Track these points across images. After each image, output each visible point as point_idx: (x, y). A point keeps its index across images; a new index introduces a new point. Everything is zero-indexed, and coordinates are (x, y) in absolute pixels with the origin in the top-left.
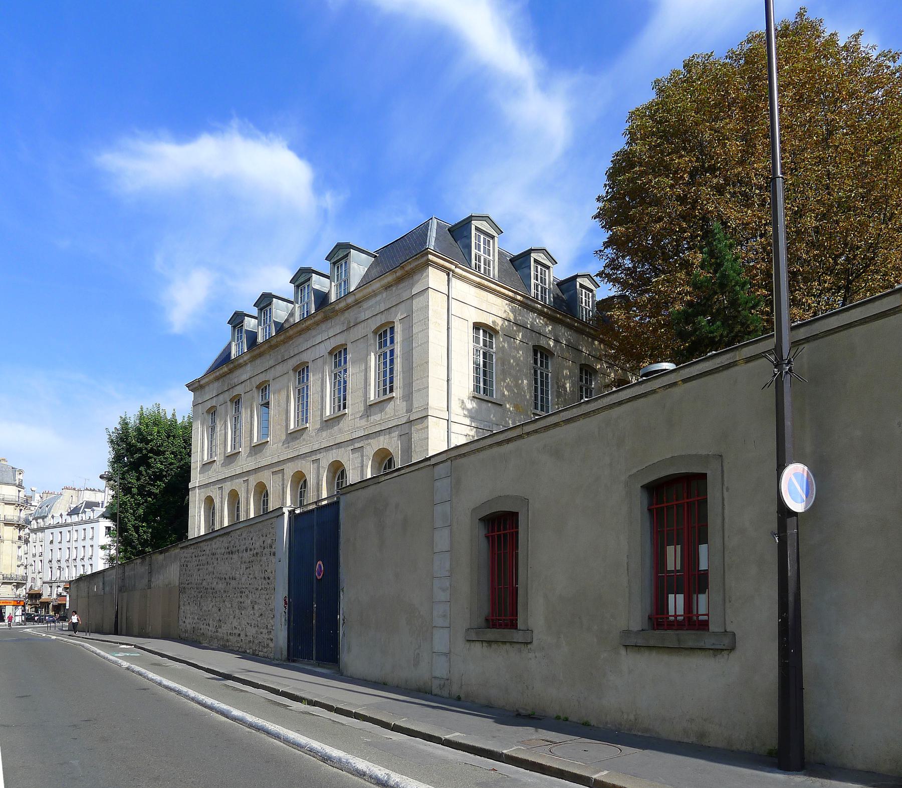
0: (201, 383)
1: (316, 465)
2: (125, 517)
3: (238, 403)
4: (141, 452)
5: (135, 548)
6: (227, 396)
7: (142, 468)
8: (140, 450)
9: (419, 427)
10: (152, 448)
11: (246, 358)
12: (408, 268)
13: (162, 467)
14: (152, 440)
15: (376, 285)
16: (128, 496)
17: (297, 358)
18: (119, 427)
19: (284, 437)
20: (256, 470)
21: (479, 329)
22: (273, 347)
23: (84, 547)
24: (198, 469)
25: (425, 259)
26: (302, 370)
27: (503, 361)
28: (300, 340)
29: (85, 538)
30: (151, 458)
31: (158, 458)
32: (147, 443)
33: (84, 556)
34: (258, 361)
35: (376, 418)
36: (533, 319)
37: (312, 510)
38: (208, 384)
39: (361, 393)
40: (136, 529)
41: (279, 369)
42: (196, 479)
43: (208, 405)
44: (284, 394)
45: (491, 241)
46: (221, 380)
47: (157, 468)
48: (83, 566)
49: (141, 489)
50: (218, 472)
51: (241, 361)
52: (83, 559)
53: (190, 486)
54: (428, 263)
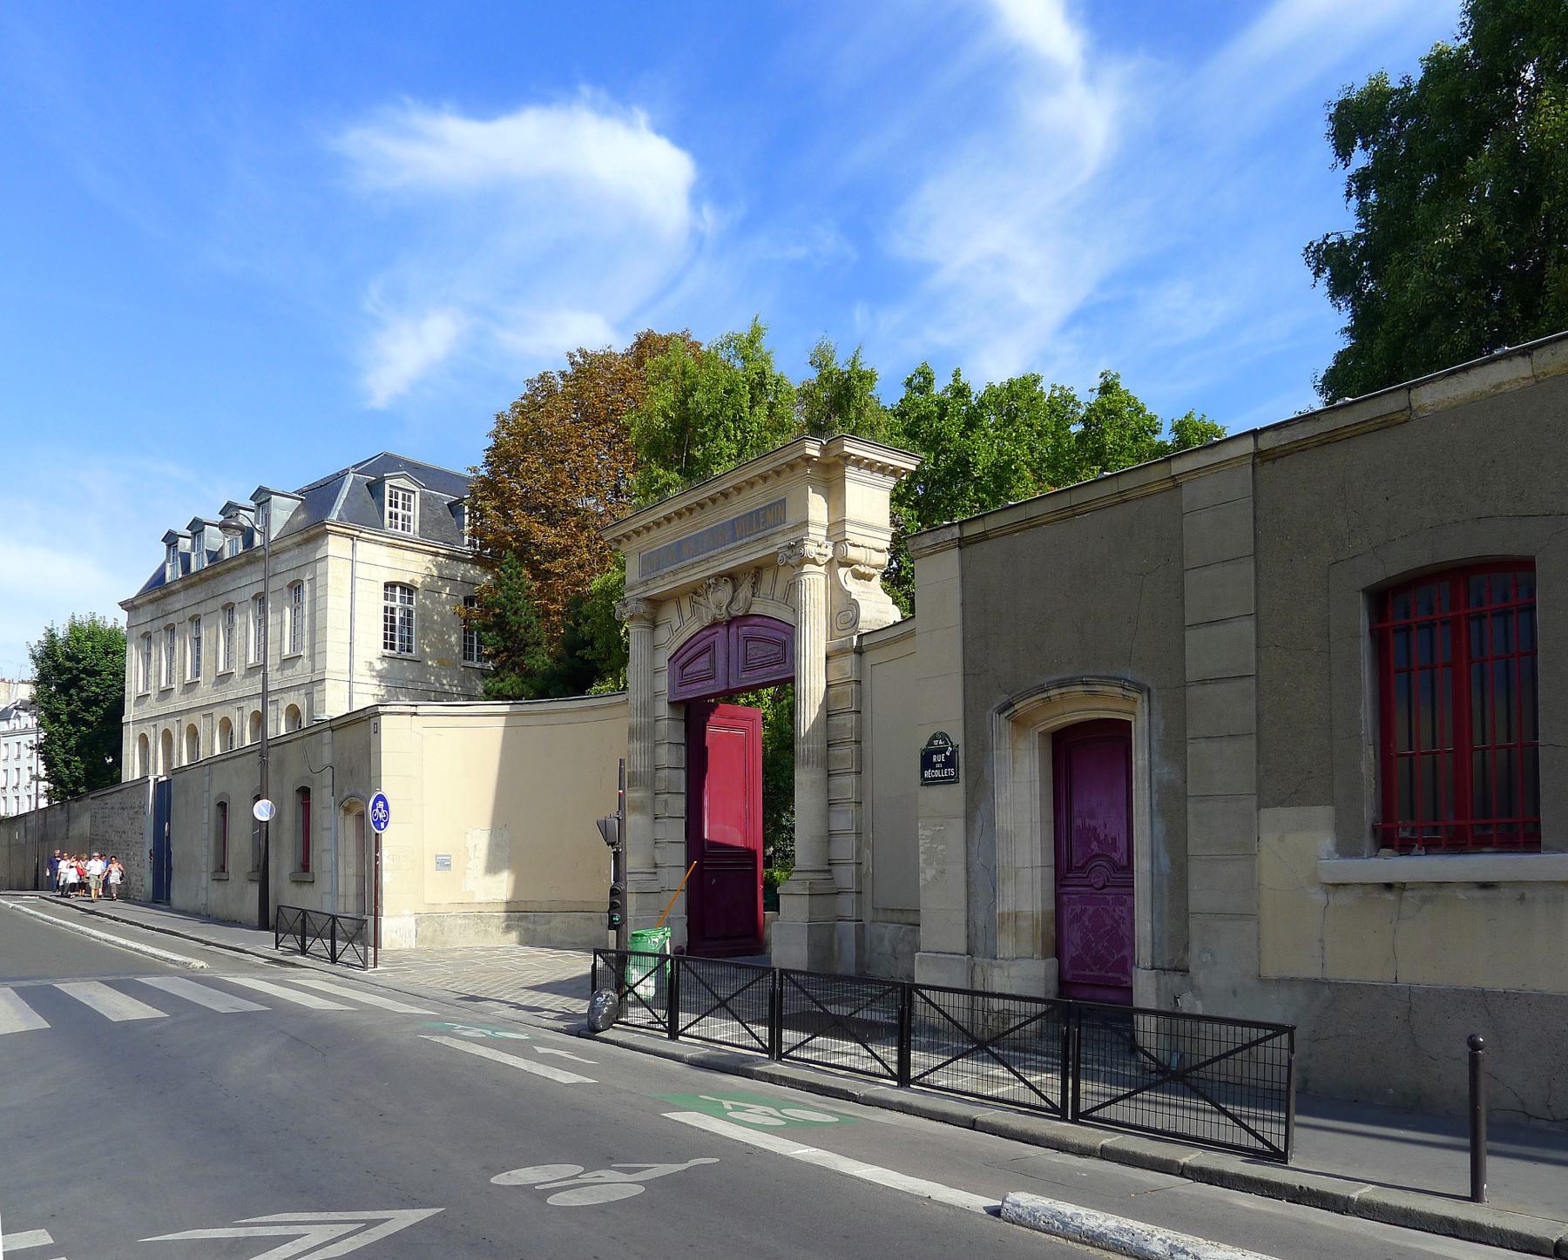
0: (135, 603)
1: (240, 712)
2: (51, 750)
3: (173, 631)
4: (71, 673)
5: (66, 787)
6: (161, 623)
7: (73, 691)
8: (70, 670)
9: (319, 688)
10: (84, 668)
11: (178, 586)
12: (312, 533)
13: (98, 690)
14: (84, 659)
15: (288, 542)
16: (56, 724)
17: (225, 596)
18: (43, 639)
19: (214, 679)
20: (189, 711)
21: (395, 587)
22: (203, 580)
23: (18, 769)
24: (133, 701)
25: (323, 528)
26: (229, 609)
27: (424, 618)
28: (227, 578)
29: (19, 756)
30: (83, 679)
31: (92, 680)
32: (78, 661)
33: (18, 784)
34: (191, 592)
35: (288, 672)
36: (461, 570)
37: (164, 782)
38: (142, 605)
39: (277, 645)
40: (67, 764)
41: (211, 605)
42: (130, 713)
43: (143, 630)
44: (214, 630)
45: (413, 496)
46: (155, 604)
47: (92, 692)
48: (17, 798)
49: (72, 715)
50: (153, 708)
51: (173, 588)
52: (16, 788)
53: (124, 720)
54: (327, 532)
